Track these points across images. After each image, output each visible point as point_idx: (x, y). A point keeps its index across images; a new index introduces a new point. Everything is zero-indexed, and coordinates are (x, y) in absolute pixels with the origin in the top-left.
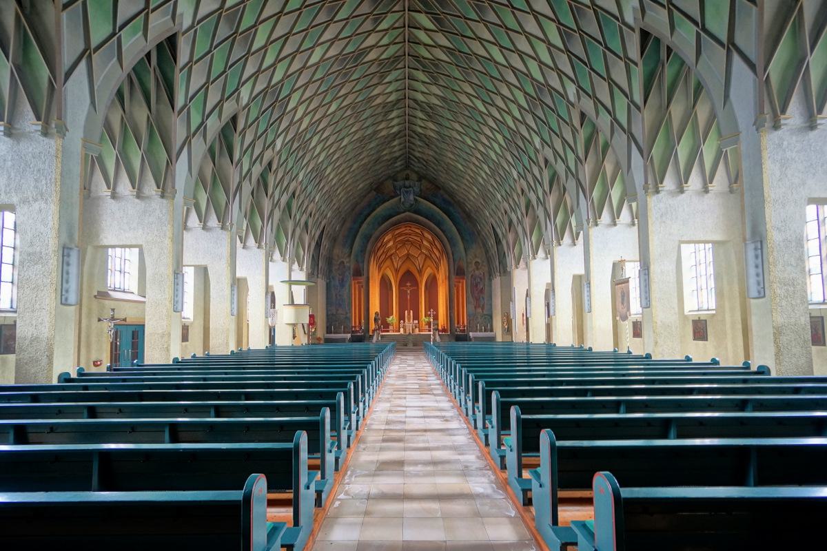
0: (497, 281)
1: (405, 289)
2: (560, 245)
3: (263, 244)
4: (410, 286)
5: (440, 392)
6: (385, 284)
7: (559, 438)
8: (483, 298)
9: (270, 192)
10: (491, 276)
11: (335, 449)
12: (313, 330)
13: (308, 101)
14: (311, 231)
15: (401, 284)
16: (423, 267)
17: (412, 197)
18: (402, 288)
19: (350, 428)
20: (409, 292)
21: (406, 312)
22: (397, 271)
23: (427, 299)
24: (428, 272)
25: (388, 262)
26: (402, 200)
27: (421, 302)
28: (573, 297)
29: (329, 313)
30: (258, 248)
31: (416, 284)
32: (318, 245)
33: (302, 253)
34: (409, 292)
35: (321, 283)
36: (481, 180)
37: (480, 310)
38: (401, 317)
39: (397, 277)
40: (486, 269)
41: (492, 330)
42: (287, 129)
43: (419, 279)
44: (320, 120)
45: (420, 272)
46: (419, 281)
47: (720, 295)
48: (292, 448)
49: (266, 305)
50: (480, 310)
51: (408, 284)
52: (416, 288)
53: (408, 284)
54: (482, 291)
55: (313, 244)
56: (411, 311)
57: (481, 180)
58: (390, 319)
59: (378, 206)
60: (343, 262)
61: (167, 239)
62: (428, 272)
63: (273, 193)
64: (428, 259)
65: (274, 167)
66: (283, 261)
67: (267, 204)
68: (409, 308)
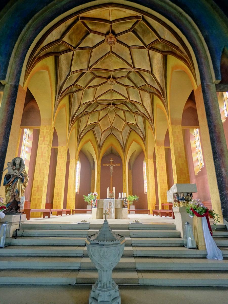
1: (107, 165)
4: (113, 163)
5: (125, 194)
7: (111, 77)
15: (105, 159)
16: (126, 142)
18: (104, 165)
20: (112, 168)
21: (108, 189)
22: (100, 147)
23: (131, 188)
24: (133, 148)
27: (125, 180)
31: (118, 159)
34: (112, 168)
38: (103, 195)
39: (99, 154)
43: (122, 156)
45: (124, 148)
47: (53, 55)
48: (132, 32)
51: (111, 161)
52: (119, 165)
53: (111, 161)
56: (114, 189)
58: (88, 197)
61: (157, 75)
62: (133, 148)
64: (133, 132)
68: (111, 184)
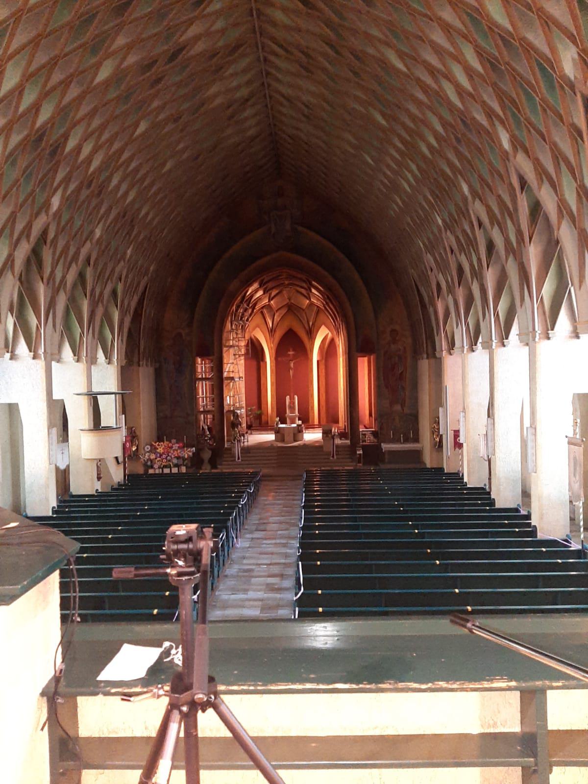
0: (424, 365)
2: (473, 351)
3: (41, 351)
6: (255, 352)
8: (403, 388)
9: (47, 270)
10: (416, 354)
11: (211, 578)
12: (134, 449)
13: (97, 134)
14: (122, 302)
15: (279, 353)
17: (288, 226)
18: (279, 359)
19: (224, 555)
21: (288, 398)
22: (272, 332)
23: (323, 374)
25: (258, 319)
26: (273, 230)
28: (161, 725)
29: (161, 414)
30: (34, 358)
32: (137, 316)
33: (110, 337)
35: (145, 376)
36: (425, 150)
37: (398, 407)
40: (410, 340)
41: (416, 440)
42: (67, 180)
44: (121, 151)
46: (308, 347)
49: (50, 444)
50: (398, 407)
51: (291, 353)
53: (291, 353)
54: (401, 377)
55: (128, 320)
57: (425, 150)
59: (331, 30)
60: (180, 335)
63: (53, 272)
65: (51, 235)
66: (78, 361)
67: (42, 291)
